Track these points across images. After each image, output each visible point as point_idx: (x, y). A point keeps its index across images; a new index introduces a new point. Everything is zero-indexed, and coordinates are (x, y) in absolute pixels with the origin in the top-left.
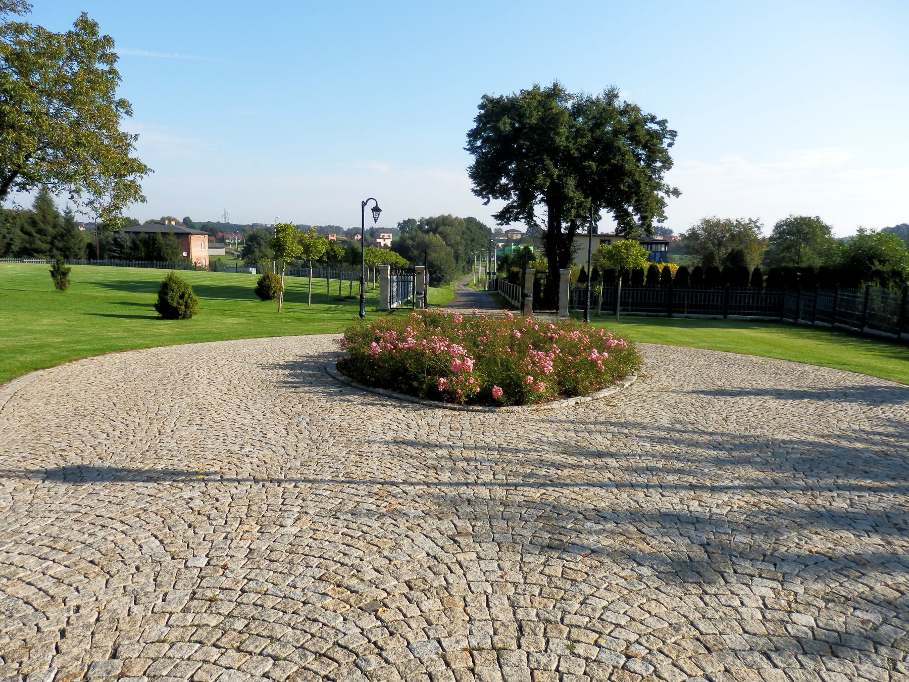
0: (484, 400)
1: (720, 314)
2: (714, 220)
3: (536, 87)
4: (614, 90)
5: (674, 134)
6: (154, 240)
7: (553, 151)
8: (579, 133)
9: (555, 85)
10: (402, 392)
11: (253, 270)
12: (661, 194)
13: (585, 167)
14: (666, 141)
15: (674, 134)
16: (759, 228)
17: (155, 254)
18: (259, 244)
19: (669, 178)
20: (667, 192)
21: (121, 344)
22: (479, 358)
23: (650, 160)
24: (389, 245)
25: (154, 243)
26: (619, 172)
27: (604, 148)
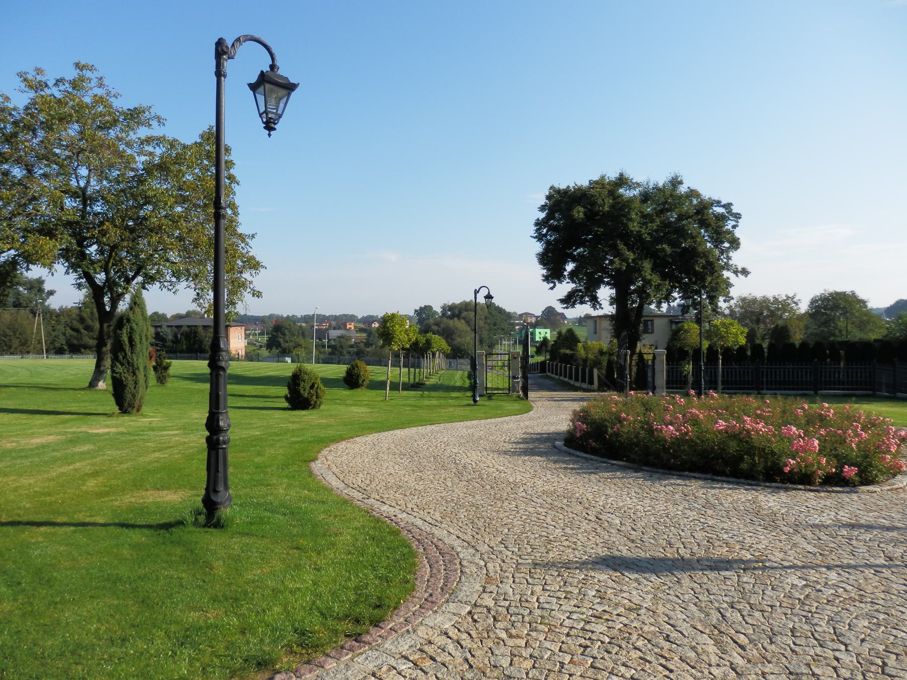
1: (810, 390)
2: (750, 297)
3: (603, 177)
4: (677, 177)
6: (195, 333)
7: (626, 236)
8: (646, 218)
9: (621, 175)
10: (727, 476)
11: (289, 360)
12: (726, 274)
13: (659, 250)
15: (738, 216)
16: (796, 304)
17: (196, 346)
18: (284, 335)
19: (737, 258)
20: (736, 272)
21: (331, 432)
23: (717, 242)
25: (195, 336)
26: (691, 254)
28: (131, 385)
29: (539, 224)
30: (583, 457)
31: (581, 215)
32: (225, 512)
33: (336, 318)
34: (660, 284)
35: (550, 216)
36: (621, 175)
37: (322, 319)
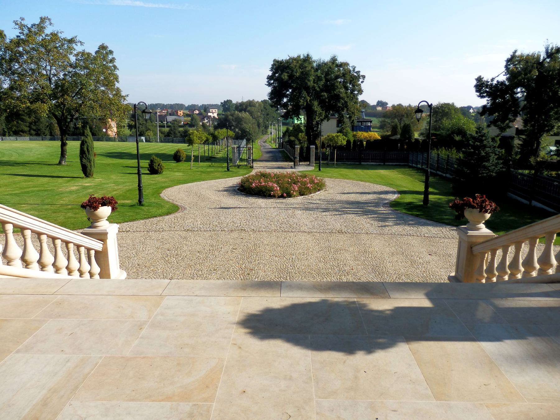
0: (282, 197)
5: (364, 77)
7: (307, 89)
8: (319, 79)
9: (308, 55)
13: (322, 96)
14: (361, 80)
15: (364, 77)
21: (166, 184)
22: (280, 187)
24: (216, 117)
27: (330, 87)
28: (89, 167)
29: (270, 78)
30: (25, 188)
31: (286, 77)
32: (143, 203)
33: (171, 106)
34: (321, 113)
35: (274, 74)
36: (308, 55)
37: (163, 107)
